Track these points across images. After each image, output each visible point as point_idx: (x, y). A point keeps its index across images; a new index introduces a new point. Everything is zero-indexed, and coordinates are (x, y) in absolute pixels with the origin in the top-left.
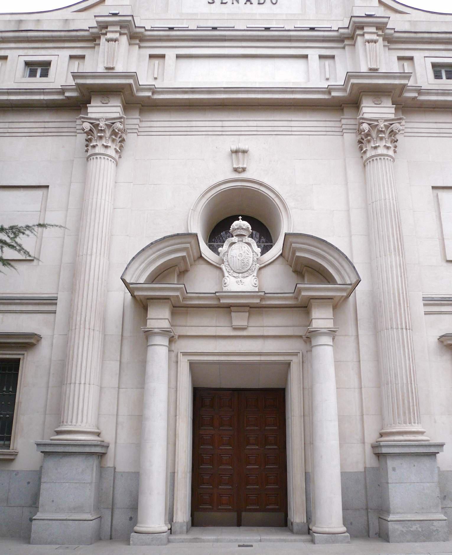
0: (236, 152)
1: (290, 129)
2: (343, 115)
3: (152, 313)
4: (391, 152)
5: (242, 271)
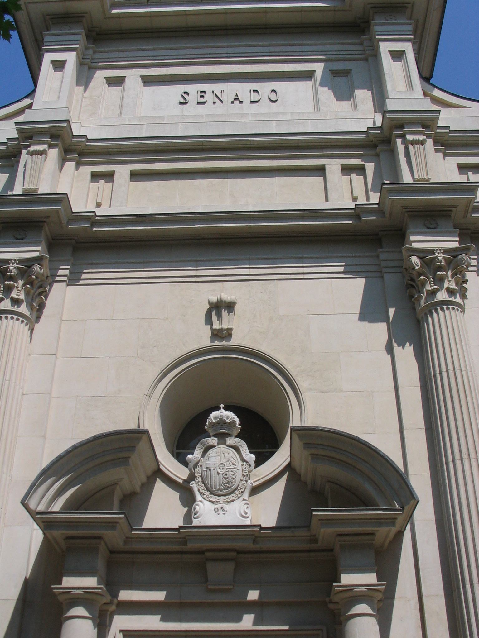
4: (458, 299)
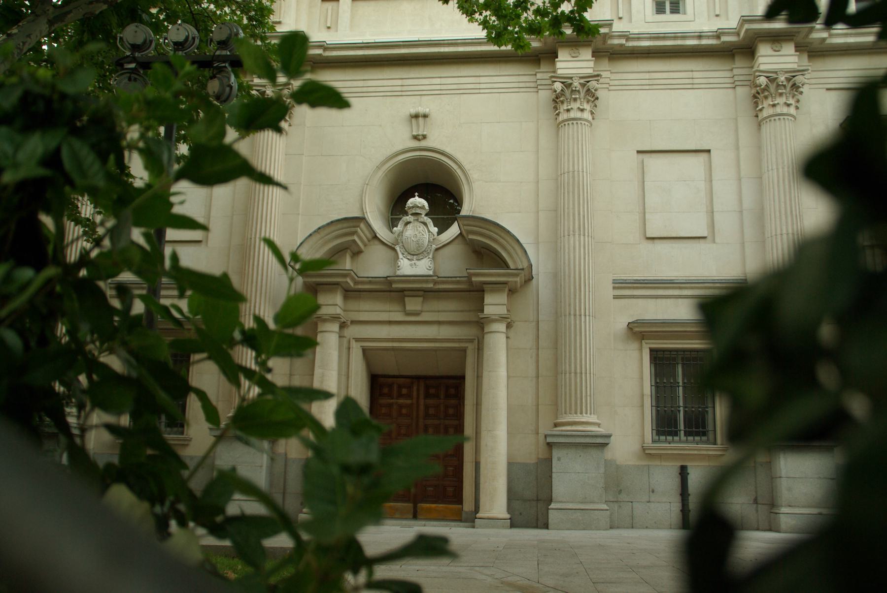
0: (416, 116)
1: (478, 86)
2: (539, 68)
3: (489, 299)
4: (792, 110)
5: (416, 254)
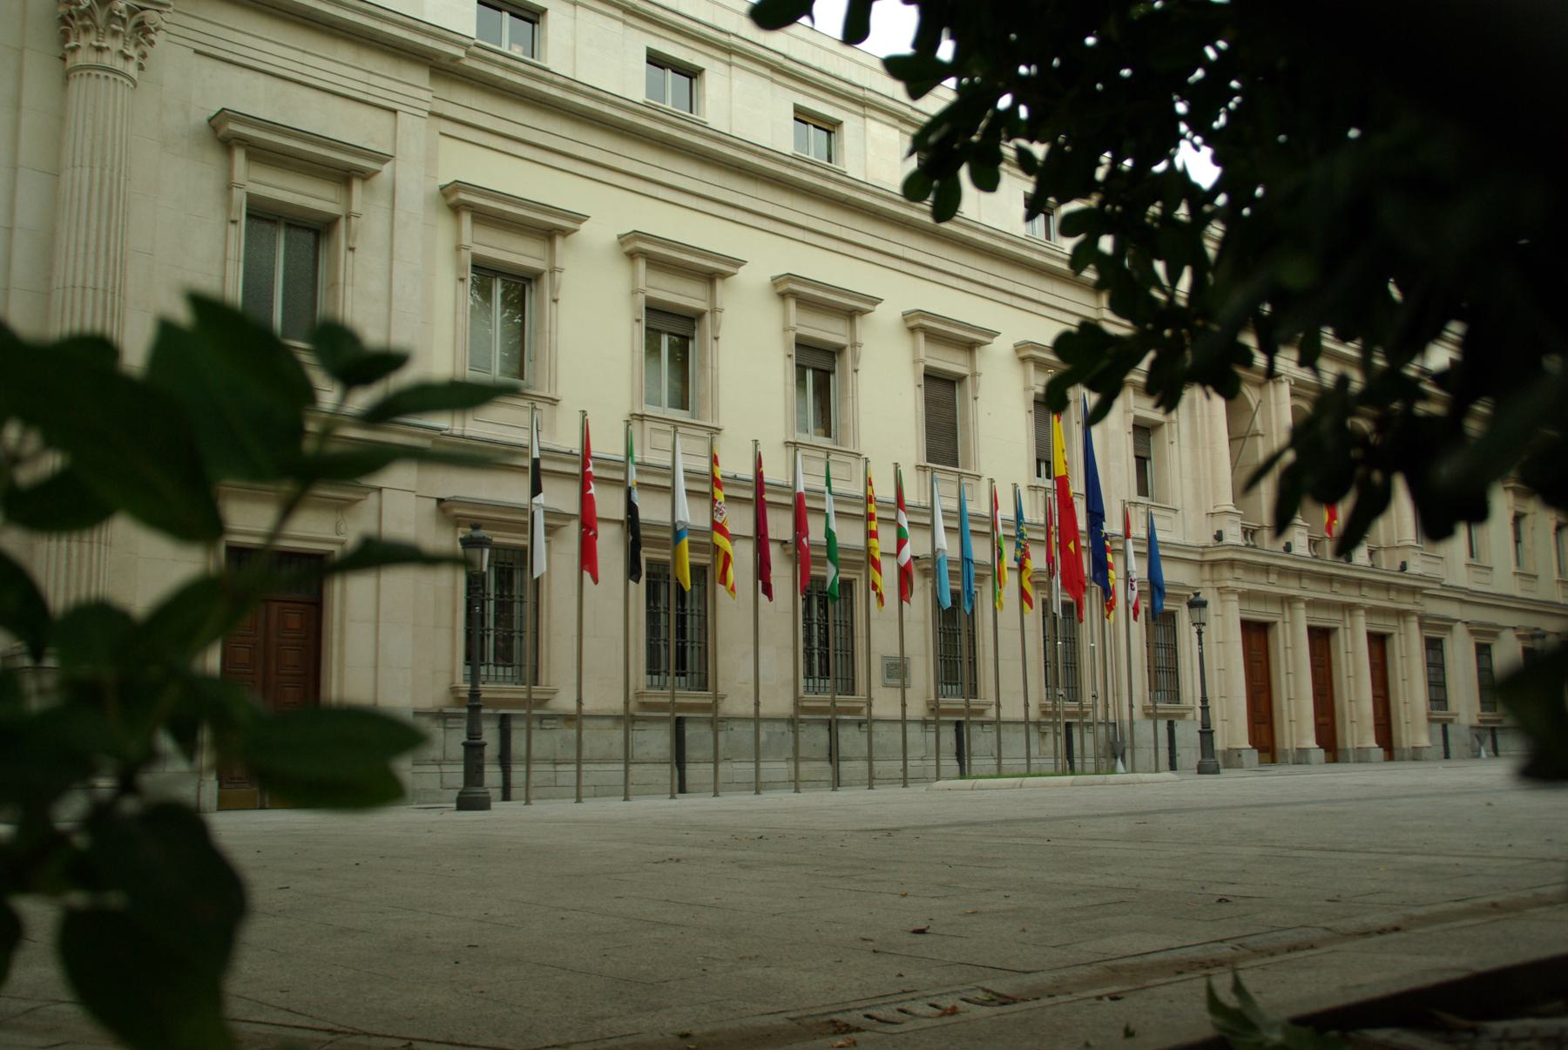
4: (131, 69)
